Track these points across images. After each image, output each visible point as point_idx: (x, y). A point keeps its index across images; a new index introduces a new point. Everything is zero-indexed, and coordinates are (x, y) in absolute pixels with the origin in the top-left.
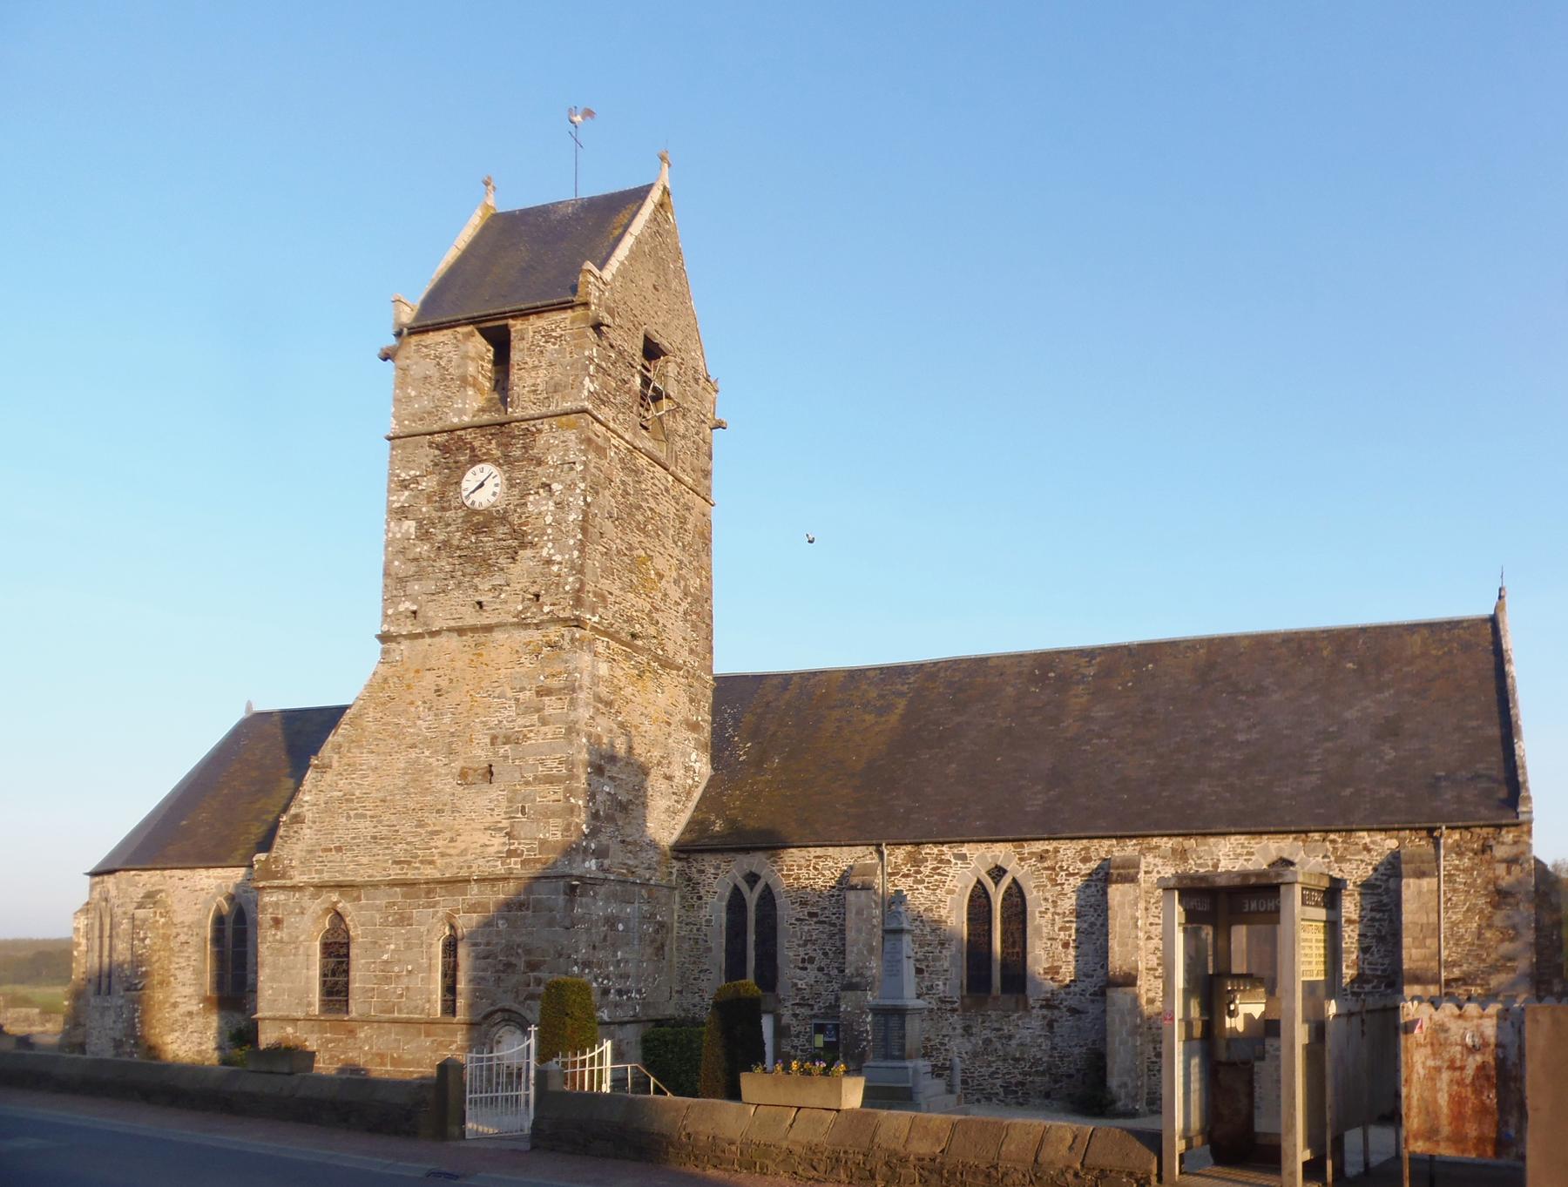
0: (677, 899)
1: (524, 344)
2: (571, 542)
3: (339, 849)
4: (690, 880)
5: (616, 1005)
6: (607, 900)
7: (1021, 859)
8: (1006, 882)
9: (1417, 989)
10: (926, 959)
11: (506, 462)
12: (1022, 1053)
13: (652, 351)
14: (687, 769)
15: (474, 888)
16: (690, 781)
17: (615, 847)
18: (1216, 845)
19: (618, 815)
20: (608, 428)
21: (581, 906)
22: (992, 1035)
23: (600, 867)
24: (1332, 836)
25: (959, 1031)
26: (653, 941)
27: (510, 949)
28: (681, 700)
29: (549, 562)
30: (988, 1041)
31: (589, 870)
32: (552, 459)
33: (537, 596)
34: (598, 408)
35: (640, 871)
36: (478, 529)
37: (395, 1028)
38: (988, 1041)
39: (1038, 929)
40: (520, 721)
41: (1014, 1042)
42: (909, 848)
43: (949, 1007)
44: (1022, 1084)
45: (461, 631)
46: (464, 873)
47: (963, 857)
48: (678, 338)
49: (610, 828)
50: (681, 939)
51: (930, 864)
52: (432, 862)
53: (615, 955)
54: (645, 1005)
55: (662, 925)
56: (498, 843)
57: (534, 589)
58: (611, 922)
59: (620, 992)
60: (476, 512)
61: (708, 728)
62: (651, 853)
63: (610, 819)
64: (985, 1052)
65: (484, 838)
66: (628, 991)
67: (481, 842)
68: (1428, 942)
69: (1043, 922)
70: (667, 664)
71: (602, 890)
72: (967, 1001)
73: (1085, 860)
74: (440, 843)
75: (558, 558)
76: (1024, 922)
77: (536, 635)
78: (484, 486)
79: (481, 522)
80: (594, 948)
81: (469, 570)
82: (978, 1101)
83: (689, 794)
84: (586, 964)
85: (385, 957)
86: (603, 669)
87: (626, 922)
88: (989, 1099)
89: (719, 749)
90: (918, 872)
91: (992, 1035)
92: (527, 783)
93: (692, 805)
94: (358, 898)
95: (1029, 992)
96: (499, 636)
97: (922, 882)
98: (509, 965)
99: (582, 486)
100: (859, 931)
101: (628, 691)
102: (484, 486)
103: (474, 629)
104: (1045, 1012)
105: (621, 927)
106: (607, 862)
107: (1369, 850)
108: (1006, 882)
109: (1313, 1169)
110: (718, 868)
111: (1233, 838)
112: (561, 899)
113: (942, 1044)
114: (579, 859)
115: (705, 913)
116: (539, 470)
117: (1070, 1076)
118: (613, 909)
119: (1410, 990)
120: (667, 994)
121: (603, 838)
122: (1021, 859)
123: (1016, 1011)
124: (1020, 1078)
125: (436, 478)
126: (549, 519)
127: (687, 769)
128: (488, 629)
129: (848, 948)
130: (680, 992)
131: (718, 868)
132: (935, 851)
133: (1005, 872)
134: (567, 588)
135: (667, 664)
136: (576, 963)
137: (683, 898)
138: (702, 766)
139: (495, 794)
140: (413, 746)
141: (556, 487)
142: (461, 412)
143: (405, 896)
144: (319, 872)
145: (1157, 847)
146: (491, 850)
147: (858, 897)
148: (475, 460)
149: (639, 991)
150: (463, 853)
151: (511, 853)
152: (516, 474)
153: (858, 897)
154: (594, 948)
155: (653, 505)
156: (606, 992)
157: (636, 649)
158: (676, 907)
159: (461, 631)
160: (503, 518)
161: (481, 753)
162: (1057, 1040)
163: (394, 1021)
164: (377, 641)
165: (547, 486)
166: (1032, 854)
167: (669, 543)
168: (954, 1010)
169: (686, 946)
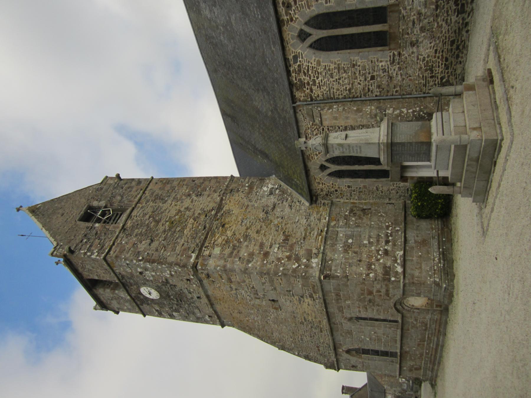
0: (338, 200)
2: (160, 267)
3: (318, 347)
4: (327, 195)
5: (394, 245)
6: (334, 251)
7: (292, 20)
8: (307, 29)
10: (364, 74)
12: (432, 3)
13: (87, 217)
16: (277, 191)
19: (290, 243)
20: (114, 244)
21: (336, 271)
22: (418, 27)
23: (317, 255)
25: (415, 49)
26: (360, 218)
28: (237, 198)
29: (172, 275)
30: (422, 29)
31: (317, 264)
33: (188, 280)
34: (104, 250)
35: (321, 227)
38: (422, 29)
41: (423, 11)
42: (294, 90)
43: (397, 58)
47: (295, 58)
48: (83, 200)
49: (297, 248)
50: (359, 198)
51: (302, 77)
52: (320, 322)
53: (365, 246)
54: (396, 223)
55: (351, 211)
56: (308, 300)
58: (347, 248)
59: (387, 242)
61: (252, 179)
62: (312, 218)
63: (292, 247)
64: (431, 30)
65: (305, 305)
66: (387, 236)
67: (307, 306)
70: (220, 207)
71: (329, 254)
72: (392, 46)
76: (335, 14)
79: (164, 296)
80: (360, 261)
82: (467, 31)
84: (369, 268)
85: (368, 339)
86: (217, 251)
87: (348, 237)
88: (467, 24)
90: (308, 84)
91: (418, 27)
93: (290, 190)
94: (341, 344)
96: (210, 293)
97: (314, 81)
99: (135, 261)
100: (347, 118)
101: (229, 234)
103: (210, 300)
105: (350, 241)
106: (314, 251)
108: (307, 29)
109: (199, 2)
110: (319, 183)
112: (333, 281)
113: (424, 60)
114: (311, 271)
118: (340, 247)
120: (390, 207)
121: (302, 252)
122: (292, 20)
123: (400, 12)
125: (154, 305)
127: (271, 193)
130: (390, 199)
131: (319, 183)
132: (293, 75)
133: (301, 30)
134: (180, 270)
135: (220, 207)
136: (368, 275)
137: (337, 198)
139: (282, 300)
141: (139, 270)
146: (311, 302)
147: (326, 120)
148: (140, 293)
149: (387, 227)
151: (311, 296)
153: (326, 120)
154: (360, 261)
155: (147, 216)
156: (386, 252)
157: (210, 229)
158: (342, 201)
159: (212, 305)
164: (225, 328)
165: (141, 273)
166: (287, 14)
167: (165, 206)
168: (399, 54)
169: (363, 197)
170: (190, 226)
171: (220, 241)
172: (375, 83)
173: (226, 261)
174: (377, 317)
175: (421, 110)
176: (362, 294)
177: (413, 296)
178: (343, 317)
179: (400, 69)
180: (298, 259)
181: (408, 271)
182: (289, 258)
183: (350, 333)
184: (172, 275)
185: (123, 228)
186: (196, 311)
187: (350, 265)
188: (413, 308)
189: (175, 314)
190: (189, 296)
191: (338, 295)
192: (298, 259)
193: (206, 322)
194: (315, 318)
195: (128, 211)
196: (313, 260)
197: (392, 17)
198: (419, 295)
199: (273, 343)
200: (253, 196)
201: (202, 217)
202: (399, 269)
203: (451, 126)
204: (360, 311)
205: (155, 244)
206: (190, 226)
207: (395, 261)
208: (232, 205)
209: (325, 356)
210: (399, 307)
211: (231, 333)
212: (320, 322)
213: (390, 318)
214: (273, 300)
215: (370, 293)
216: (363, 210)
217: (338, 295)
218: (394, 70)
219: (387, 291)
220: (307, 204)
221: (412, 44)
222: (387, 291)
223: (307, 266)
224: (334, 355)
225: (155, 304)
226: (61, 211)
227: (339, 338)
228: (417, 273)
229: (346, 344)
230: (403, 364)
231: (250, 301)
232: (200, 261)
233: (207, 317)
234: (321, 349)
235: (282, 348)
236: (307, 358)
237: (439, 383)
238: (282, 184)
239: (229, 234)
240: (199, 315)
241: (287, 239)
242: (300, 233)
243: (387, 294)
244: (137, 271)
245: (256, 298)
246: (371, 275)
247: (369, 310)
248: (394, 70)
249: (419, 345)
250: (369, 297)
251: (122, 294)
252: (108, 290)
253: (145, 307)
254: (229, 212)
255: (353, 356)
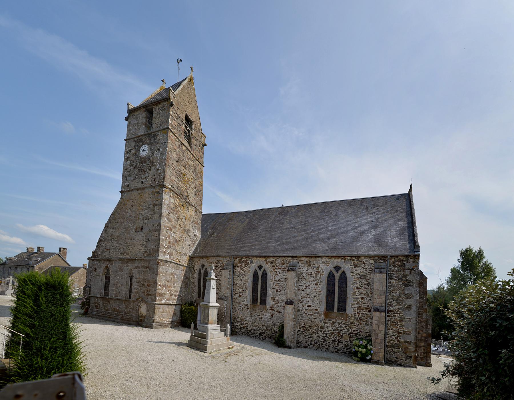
1: (156, 112)
3: (109, 250)
6: (172, 268)
9: (73, 304)
11: (150, 144)
14: (195, 235)
15: (137, 262)
17: (174, 253)
18: (319, 260)
19: (175, 244)
23: (170, 258)
24: (353, 258)
25: (249, 315)
27: (144, 280)
29: (158, 170)
30: (256, 319)
32: (160, 142)
33: (155, 179)
36: (143, 162)
37: (118, 301)
38: (256, 319)
39: (270, 285)
40: (149, 213)
44: (264, 333)
45: (137, 189)
46: (135, 258)
47: (252, 262)
51: (244, 263)
52: (128, 254)
56: (143, 249)
57: (154, 177)
60: (143, 158)
65: (140, 247)
68: (382, 297)
69: (271, 283)
71: (171, 265)
73: (283, 264)
74: (130, 249)
75: (160, 168)
77: (154, 190)
78: (144, 151)
79: (143, 160)
80: (168, 281)
81: (141, 173)
83: (195, 242)
84: (164, 286)
86: (172, 201)
88: (256, 337)
89: (203, 231)
92: (150, 231)
93: (196, 245)
94: (112, 264)
95: (267, 304)
96: (146, 190)
98: (143, 285)
101: (179, 208)
102: (144, 151)
103: (140, 189)
104: (271, 311)
106: (172, 257)
107: (364, 264)
111: (324, 258)
115: (195, 275)
116: (157, 145)
117: (276, 332)
119: (73, 304)
124: (264, 331)
125: (135, 149)
126: (159, 158)
127: (195, 235)
128: (143, 188)
129: (222, 288)
135: (190, 205)
138: (199, 235)
139: (142, 234)
140: (126, 221)
141: (161, 149)
142: (141, 132)
143: (122, 263)
144: (105, 256)
145: (302, 260)
146: (142, 251)
148: (143, 144)
150: (135, 251)
151: (146, 252)
152: (152, 147)
154: (168, 281)
156: (171, 295)
159: (137, 189)
160: (149, 159)
161: (140, 223)
162: (273, 320)
163: (117, 299)
165: (159, 149)
167: (191, 172)
170: (183, 186)
171: (177, 203)
172: (238, 297)
173: (168, 205)
174: (133, 288)
175: (225, 316)
176: (148, 281)
177: (147, 308)
178: (132, 268)
179: (243, 308)
180: (169, 247)
181: (162, 306)
182: (169, 242)
183: (121, 271)
184: (158, 170)
185: (182, 144)
186: (132, 178)
187: (165, 276)
188: (139, 308)
189: (129, 162)
190: (143, 177)
191: (147, 267)
192: (169, 247)
193: (123, 182)
194: (131, 252)
195: (189, 148)
196: (168, 256)
197: (261, 307)
198: (148, 311)
199: (110, 221)
200: (194, 224)
201: (186, 194)
202: (163, 302)
203: (215, 333)
204: (136, 278)
205: (175, 162)
206: (183, 186)
207: (168, 299)
208: (191, 212)
209: (102, 253)
210: (140, 300)
211: (118, 197)
212: (128, 254)
213: (132, 295)
214: (142, 229)
215: (149, 286)
216: (187, 284)
217: (147, 267)
218: (242, 306)
219: (150, 295)
220: (190, 255)
221: (251, 314)
222: (150, 295)
223: (165, 252)
224: (104, 259)
225: (136, 151)
226: (190, 101)
227: (117, 264)
228: (161, 310)
229: (113, 268)
230: (99, 299)
231: (141, 214)
232: (168, 190)
233: (127, 183)
234: (108, 251)
235: (106, 226)
236: (100, 241)
237: (85, 318)
238: (198, 242)
239: (179, 208)
240: (129, 178)
241: (177, 242)
242: (179, 249)
243: (148, 295)
244: (160, 147)
245: (143, 218)
246: (160, 287)
247: (137, 284)
248: (242, 306)
249: (115, 309)
250: (146, 285)
251: (142, 131)
252: (144, 120)
253: (133, 144)
254: (188, 210)
255: (104, 270)
